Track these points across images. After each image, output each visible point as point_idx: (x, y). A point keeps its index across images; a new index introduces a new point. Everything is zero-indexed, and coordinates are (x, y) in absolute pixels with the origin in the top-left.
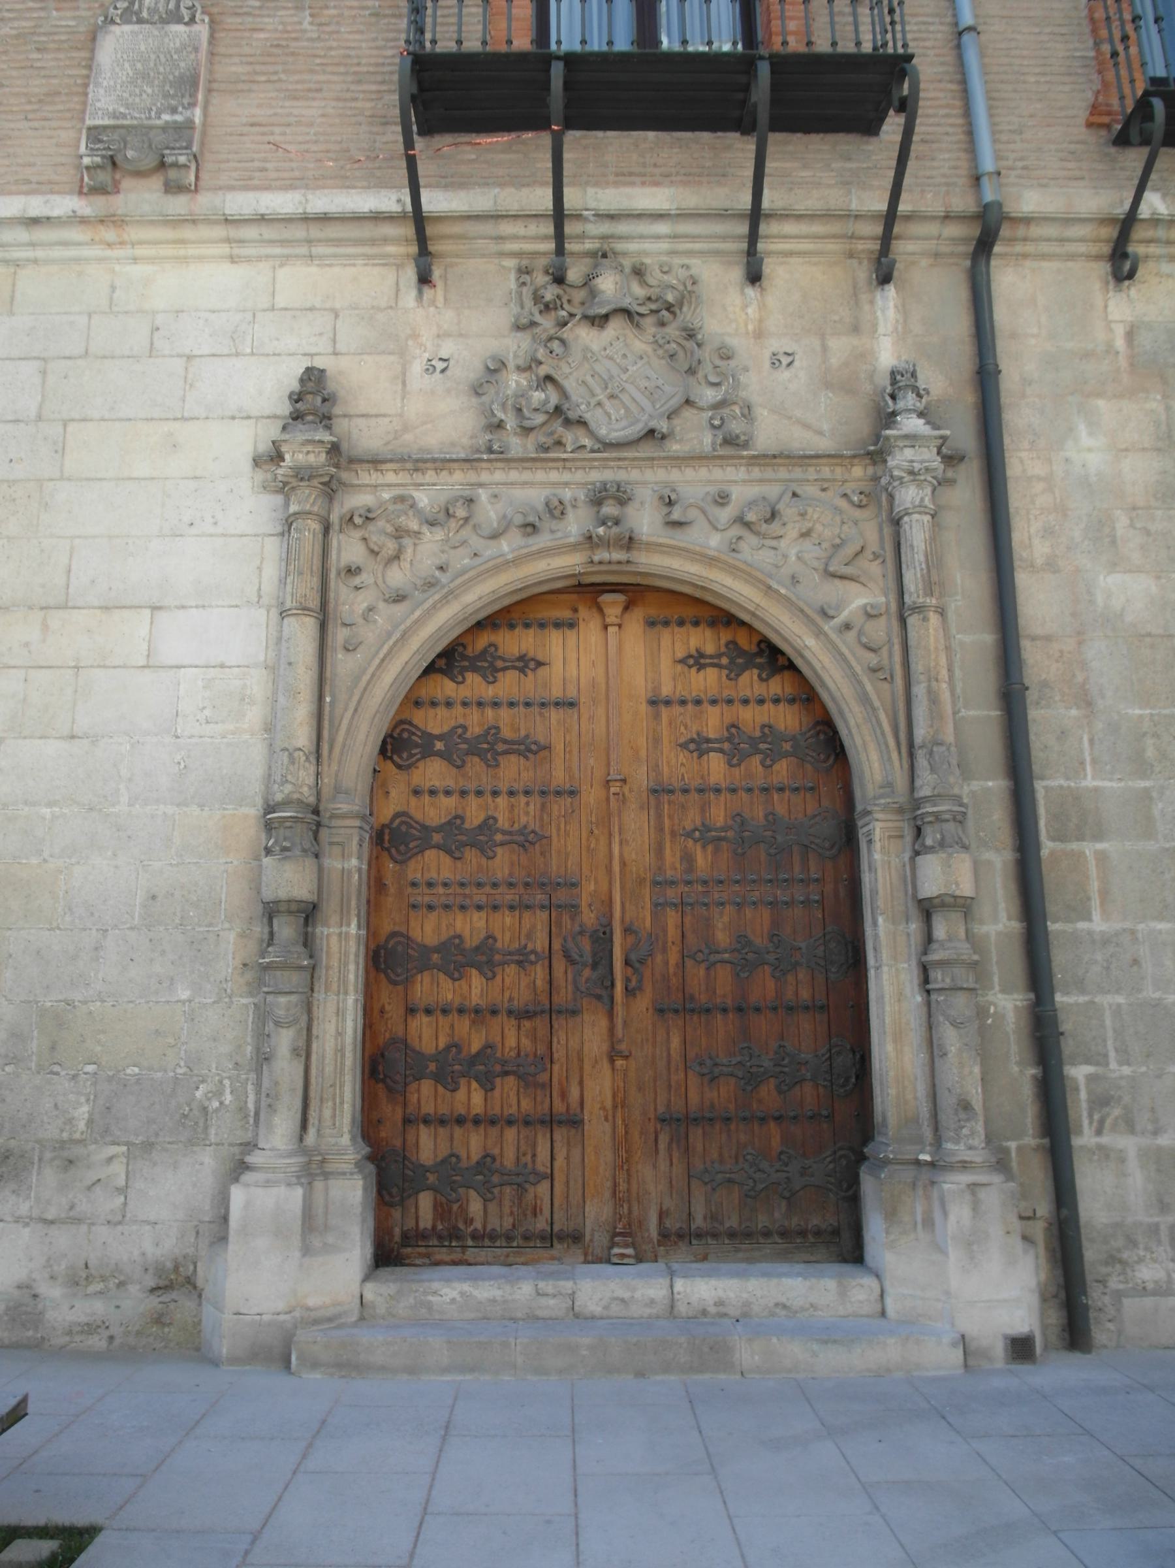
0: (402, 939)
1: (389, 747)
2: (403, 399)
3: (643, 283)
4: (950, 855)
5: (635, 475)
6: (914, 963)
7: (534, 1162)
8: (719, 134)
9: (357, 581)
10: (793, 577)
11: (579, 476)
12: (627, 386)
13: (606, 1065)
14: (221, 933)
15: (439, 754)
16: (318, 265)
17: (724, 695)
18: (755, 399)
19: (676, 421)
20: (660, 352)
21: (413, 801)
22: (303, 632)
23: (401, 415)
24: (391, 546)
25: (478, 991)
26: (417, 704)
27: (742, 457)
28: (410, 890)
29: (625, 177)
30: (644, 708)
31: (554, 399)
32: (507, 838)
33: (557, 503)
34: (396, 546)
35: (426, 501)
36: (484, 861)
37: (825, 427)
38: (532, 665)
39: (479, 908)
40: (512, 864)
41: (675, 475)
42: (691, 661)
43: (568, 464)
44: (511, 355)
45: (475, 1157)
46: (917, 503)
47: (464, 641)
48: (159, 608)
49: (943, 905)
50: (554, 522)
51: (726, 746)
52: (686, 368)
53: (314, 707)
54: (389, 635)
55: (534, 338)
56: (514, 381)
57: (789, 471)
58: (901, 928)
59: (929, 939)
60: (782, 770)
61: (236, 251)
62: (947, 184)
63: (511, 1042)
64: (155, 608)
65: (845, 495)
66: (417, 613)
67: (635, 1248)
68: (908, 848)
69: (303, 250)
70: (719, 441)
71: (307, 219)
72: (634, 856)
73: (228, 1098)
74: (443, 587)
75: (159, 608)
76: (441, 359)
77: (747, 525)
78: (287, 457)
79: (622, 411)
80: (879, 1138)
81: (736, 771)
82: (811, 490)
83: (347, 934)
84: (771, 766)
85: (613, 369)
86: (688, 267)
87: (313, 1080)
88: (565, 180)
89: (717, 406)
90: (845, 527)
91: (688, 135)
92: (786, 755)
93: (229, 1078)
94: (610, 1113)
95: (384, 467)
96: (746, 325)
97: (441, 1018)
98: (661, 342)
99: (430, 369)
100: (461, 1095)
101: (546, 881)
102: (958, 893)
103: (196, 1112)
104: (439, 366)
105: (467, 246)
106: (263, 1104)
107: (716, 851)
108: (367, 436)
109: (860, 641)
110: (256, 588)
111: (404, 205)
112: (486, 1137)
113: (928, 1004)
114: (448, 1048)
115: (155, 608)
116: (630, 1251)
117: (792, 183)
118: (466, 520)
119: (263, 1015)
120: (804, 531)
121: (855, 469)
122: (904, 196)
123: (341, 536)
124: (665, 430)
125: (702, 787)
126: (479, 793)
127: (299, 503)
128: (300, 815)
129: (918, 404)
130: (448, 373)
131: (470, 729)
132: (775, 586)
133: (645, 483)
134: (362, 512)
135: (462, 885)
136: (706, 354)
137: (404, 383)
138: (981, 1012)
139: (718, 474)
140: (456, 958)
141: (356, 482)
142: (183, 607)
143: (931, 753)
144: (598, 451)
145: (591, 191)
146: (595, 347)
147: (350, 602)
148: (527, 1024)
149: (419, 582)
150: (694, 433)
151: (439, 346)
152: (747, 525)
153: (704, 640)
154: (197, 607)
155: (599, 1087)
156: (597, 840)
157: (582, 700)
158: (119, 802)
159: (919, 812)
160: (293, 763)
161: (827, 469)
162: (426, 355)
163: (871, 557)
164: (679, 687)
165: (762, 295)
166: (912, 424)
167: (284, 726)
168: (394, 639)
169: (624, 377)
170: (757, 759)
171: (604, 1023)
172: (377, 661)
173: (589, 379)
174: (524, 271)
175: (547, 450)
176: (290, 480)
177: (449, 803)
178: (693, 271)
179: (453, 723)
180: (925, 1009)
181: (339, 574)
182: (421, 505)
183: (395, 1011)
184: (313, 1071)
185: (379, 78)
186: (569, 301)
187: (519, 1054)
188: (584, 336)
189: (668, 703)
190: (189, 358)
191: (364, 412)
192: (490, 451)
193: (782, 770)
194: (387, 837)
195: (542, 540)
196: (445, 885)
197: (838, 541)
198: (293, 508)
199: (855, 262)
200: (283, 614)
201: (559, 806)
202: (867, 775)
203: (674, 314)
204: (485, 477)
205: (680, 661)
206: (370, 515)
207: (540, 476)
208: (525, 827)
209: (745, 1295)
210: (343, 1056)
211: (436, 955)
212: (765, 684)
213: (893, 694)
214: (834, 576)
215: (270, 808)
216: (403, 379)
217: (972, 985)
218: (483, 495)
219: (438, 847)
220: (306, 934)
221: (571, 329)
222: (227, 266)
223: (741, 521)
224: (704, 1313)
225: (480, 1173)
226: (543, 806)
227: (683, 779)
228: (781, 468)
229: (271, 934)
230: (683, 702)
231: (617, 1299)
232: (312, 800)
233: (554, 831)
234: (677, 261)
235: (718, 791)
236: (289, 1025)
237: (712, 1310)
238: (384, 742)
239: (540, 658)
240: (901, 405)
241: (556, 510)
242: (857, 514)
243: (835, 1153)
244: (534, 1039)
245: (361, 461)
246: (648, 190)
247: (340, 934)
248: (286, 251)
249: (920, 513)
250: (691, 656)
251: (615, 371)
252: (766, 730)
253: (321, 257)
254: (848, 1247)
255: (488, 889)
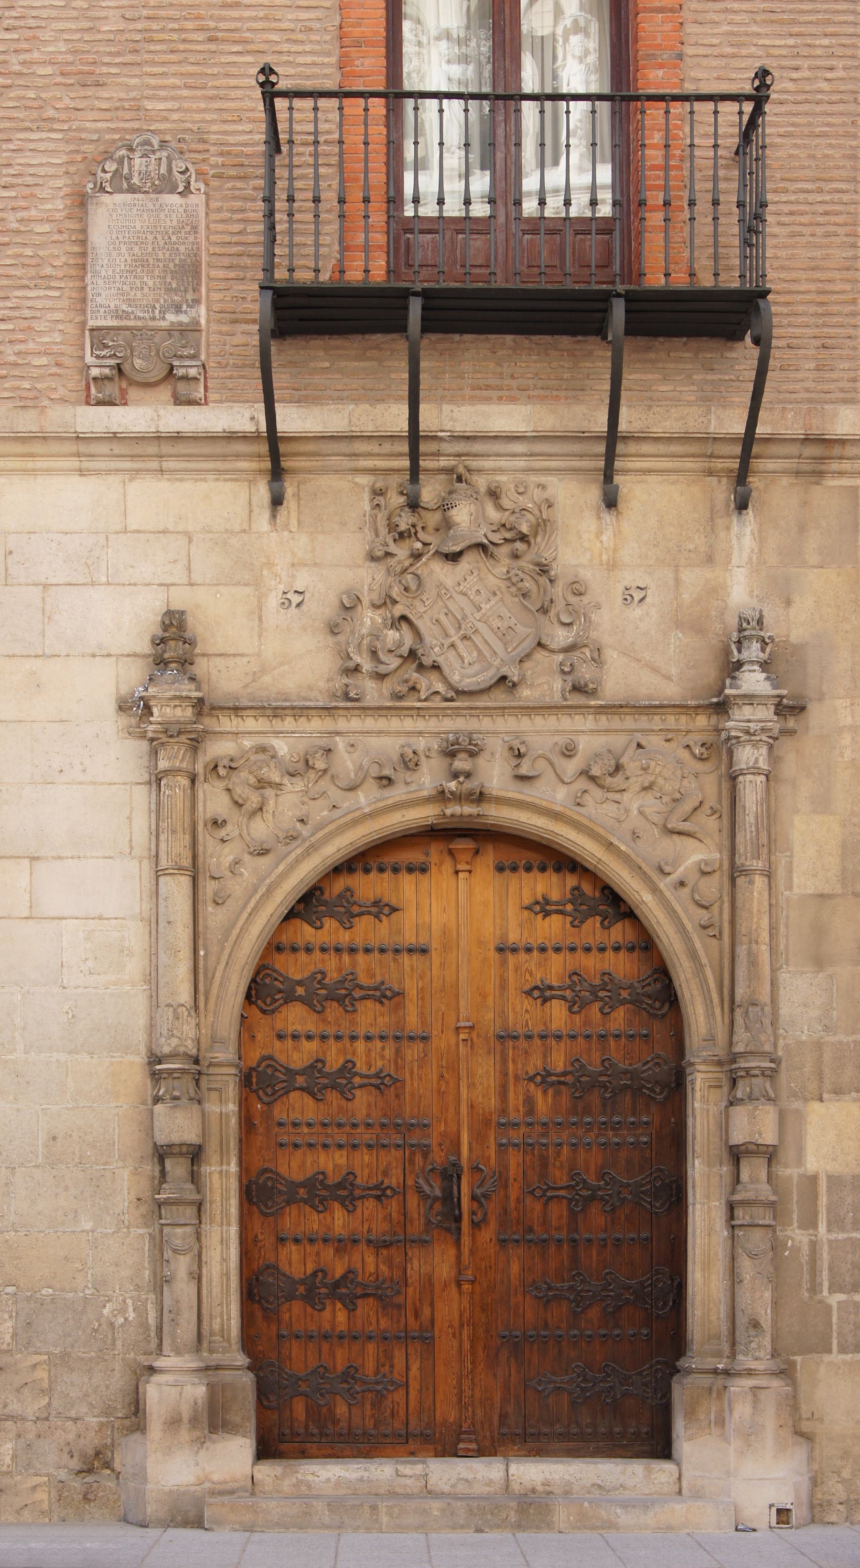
0: (271, 1175)
1: (253, 993)
2: (260, 636)
3: (500, 508)
4: (756, 1108)
5: (486, 723)
6: (723, 1202)
7: (391, 1372)
8: (579, 338)
9: (223, 833)
10: (634, 833)
11: (433, 725)
12: (480, 626)
13: (454, 1288)
14: (116, 1171)
15: (300, 999)
16: (169, 480)
17: (568, 943)
18: (606, 640)
19: (527, 665)
20: (513, 589)
21: (277, 1044)
22: (177, 889)
23: (259, 655)
24: (254, 799)
25: (341, 1223)
26: (279, 949)
27: (590, 707)
28: (277, 1129)
29: (483, 392)
30: (493, 955)
31: (409, 640)
32: (366, 1081)
33: (411, 755)
34: (260, 799)
35: (286, 749)
36: (344, 1103)
37: (674, 671)
38: (386, 910)
39: (340, 1146)
40: (369, 1105)
41: (525, 724)
42: (537, 908)
43: (422, 713)
44: (366, 588)
45: (340, 1368)
46: (751, 764)
47: (322, 885)
48: (37, 858)
49: (748, 1152)
50: (409, 773)
51: (568, 994)
52: (538, 607)
53: (192, 963)
54: (255, 890)
55: (388, 571)
56: (369, 618)
57: (635, 720)
58: (715, 1170)
59: (737, 1180)
60: (619, 1018)
61: (86, 465)
62: (810, 401)
63: (371, 1268)
64: (34, 859)
65: (688, 746)
66: (281, 868)
67: (478, 1444)
68: (725, 1098)
69: (154, 465)
70: (569, 687)
71: (158, 438)
72: (480, 1099)
73: (131, 1315)
74: (304, 840)
75: (37, 858)
76: (296, 592)
77: (593, 779)
78: (155, 710)
79: (475, 654)
80: (689, 1354)
81: (577, 1018)
82: (654, 741)
83: (227, 1172)
84: (609, 1013)
85: (468, 611)
86: (543, 487)
87: (204, 1300)
88: (422, 394)
89: (569, 649)
90: (685, 781)
91: (548, 338)
92: (623, 1002)
93: (131, 1297)
94: (457, 1331)
95: (244, 713)
96: (601, 556)
97: (308, 1248)
98: (514, 580)
99: (286, 604)
100: (327, 1314)
101: (400, 1121)
102: (760, 1142)
103: (104, 1326)
104: (295, 600)
105: (320, 463)
106: (166, 1319)
107: (557, 1094)
108: (225, 677)
109: (693, 899)
110: (128, 838)
111: (257, 424)
112: (350, 1349)
113: (733, 1237)
114: (315, 1274)
115: (34, 859)
116: (473, 1446)
117: (651, 399)
118: (325, 771)
119: (159, 1244)
120: (646, 784)
121: (699, 717)
122: (762, 414)
123: (206, 785)
124: (515, 679)
125: (544, 1033)
126: (338, 1038)
127: (169, 759)
128: (186, 1067)
129: (761, 655)
130: (304, 607)
131: (329, 975)
132: (616, 842)
133: (496, 733)
134: (226, 762)
135: (324, 1125)
136: (559, 591)
137: (260, 619)
138: (776, 1247)
139: (566, 723)
140: (319, 1192)
141: (218, 729)
142: (60, 858)
143: (747, 1013)
144: (451, 700)
145: (446, 408)
146: (449, 582)
147: (219, 856)
148: (385, 1252)
149: (281, 835)
150: (544, 682)
151: (293, 576)
152: (593, 779)
153: (549, 885)
154: (72, 858)
155: (449, 1308)
156: (447, 1083)
157: (434, 946)
158: (15, 1050)
159: (734, 1066)
160: (178, 1018)
161: (672, 717)
162: (282, 588)
163: (709, 812)
164: (526, 934)
165: (617, 519)
166: (753, 681)
167: (167, 983)
168: (260, 893)
169: (478, 616)
170: (597, 1006)
171: (452, 1252)
172: (245, 915)
173: (443, 618)
174: (378, 493)
175: (399, 697)
176: (160, 736)
177: (311, 1048)
178: (549, 493)
179: (312, 968)
180: (730, 1242)
181: (205, 825)
182: (281, 753)
183: (267, 1240)
184: (204, 1292)
185: (226, 261)
186: (423, 528)
187: (377, 1278)
188: (439, 572)
189: (514, 950)
190: (46, 586)
191: (222, 652)
192: (347, 697)
193: (619, 1018)
194: (254, 1080)
195: (397, 793)
196: (309, 1125)
197: (678, 796)
198: (163, 764)
199: (714, 480)
200: (158, 873)
201: (413, 1052)
202: (693, 1027)
203: (528, 543)
204: (342, 724)
205: (527, 908)
206: (233, 765)
207: (395, 723)
208: (381, 1071)
209: (567, 1477)
210: (228, 1280)
211: (302, 1190)
212: (606, 931)
213: (721, 952)
214: (673, 832)
215: (154, 1059)
216: (258, 613)
217: (767, 1222)
218: (340, 743)
219: (302, 1089)
220: (192, 1171)
221: (426, 564)
222: (76, 479)
223: (585, 773)
224: (534, 1491)
225: (346, 1382)
226: (398, 1051)
227: (527, 1025)
228: (628, 717)
229: (163, 1173)
230: (529, 950)
231: (462, 1479)
232: (194, 1052)
233: (407, 1074)
234: (534, 479)
235: (559, 1037)
236: (184, 1252)
237: (540, 1488)
238: (250, 988)
239: (394, 902)
240: (745, 655)
241: (410, 763)
242: (699, 766)
243: (651, 1367)
244: (391, 1267)
245: (221, 708)
246: (505, 408)
247: (221, 1172)
248: (135, 465)
249: (753, 774)
250: (537, 903)
251: (468, 610)
252: (606, 978)
253: (172, 471)
254: (660, 1446)
255: (347, 1129)
